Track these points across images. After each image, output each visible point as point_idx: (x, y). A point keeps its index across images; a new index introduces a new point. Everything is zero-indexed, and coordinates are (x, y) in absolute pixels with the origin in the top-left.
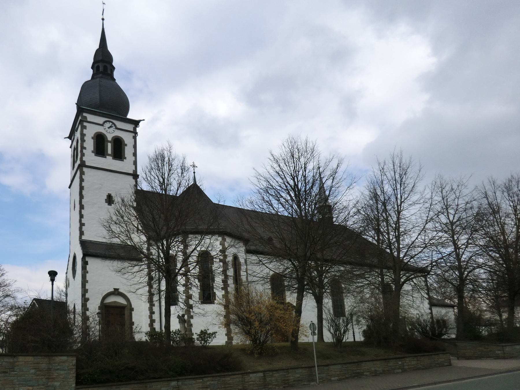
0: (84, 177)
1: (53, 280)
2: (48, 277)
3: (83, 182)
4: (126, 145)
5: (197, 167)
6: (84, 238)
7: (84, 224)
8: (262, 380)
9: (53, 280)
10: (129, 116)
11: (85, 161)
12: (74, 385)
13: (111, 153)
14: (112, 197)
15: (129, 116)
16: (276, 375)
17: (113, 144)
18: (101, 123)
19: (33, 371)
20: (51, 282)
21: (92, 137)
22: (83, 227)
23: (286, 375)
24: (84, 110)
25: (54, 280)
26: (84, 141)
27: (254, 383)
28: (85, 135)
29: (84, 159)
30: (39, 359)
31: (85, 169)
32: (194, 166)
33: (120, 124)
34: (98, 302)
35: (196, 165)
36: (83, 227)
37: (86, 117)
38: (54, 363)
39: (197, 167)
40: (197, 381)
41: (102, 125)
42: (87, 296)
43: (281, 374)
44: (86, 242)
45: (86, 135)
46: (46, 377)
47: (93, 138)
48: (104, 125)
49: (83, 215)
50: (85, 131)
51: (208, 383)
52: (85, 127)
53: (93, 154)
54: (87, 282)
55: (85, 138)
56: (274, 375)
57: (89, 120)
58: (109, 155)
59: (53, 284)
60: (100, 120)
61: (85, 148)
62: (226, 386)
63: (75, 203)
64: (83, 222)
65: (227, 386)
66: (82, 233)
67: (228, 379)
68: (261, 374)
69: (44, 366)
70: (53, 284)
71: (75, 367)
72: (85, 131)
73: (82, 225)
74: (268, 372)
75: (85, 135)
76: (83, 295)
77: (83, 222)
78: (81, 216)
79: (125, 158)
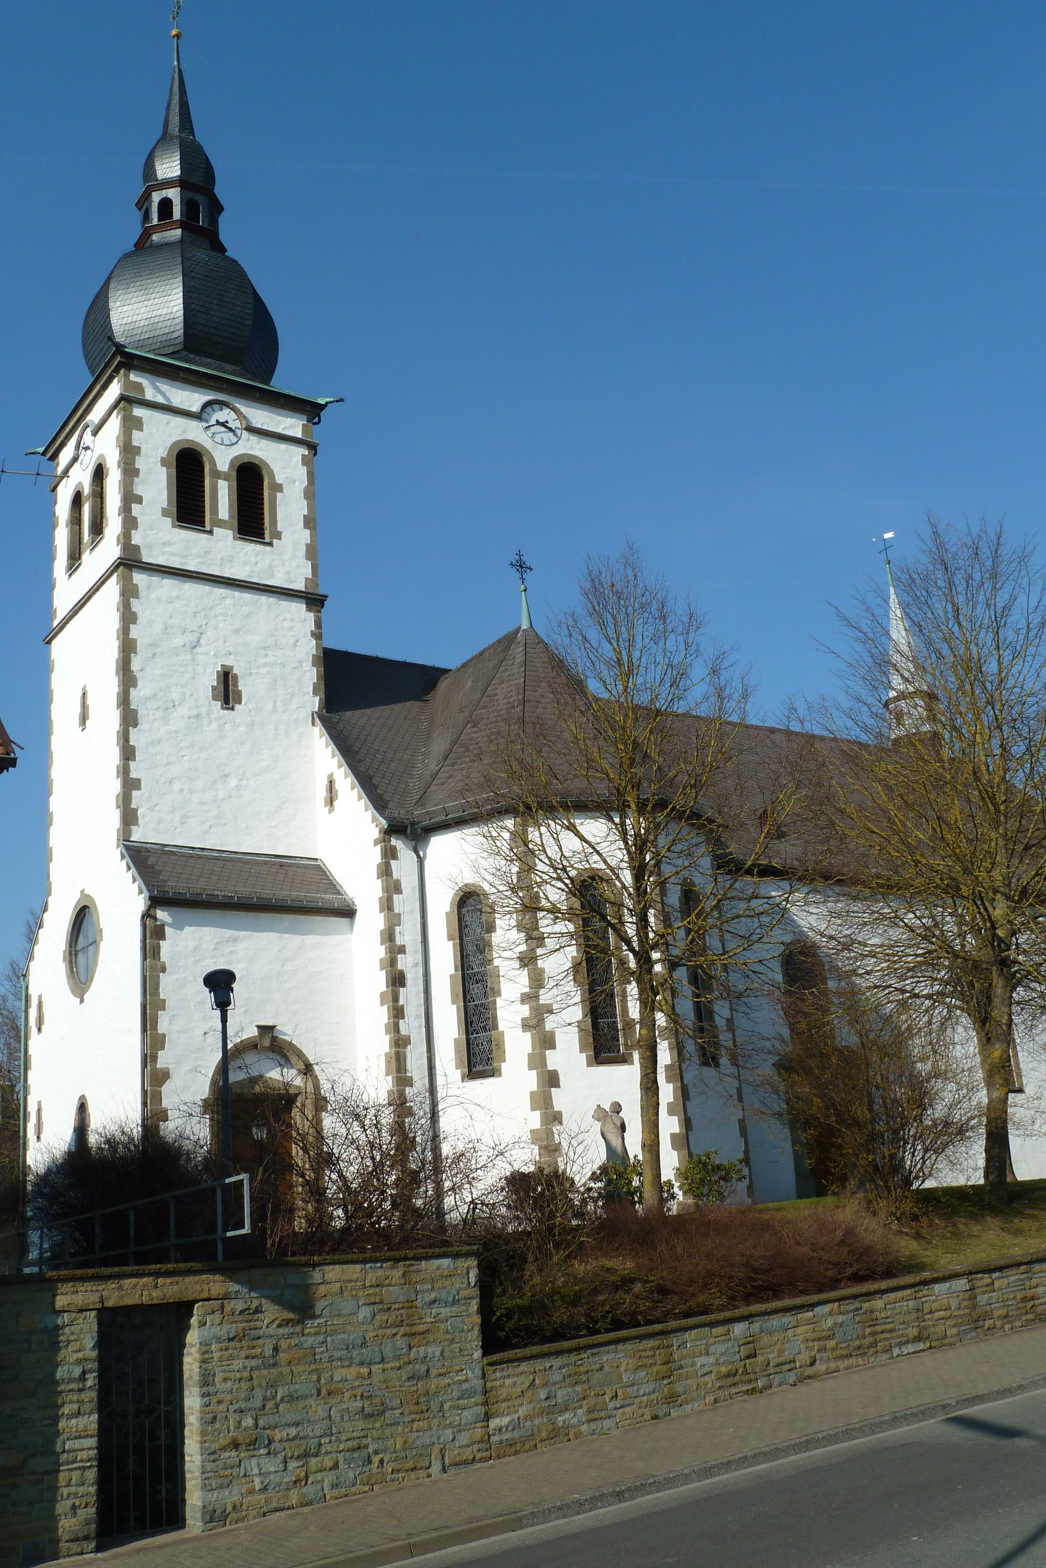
0: (135, 605)
1: (223, 1004)
2: (207, 997)
3: (135, 623)
4: (279, 488)
5: (512, 564)
6: (138, 835)
7: (139, 781)
8: (965, 1303)
9: (223, 1004)
10: (279, 383)
11: (137, 548)
12: (478, 1354)
13: (230, 516)
14: (236, 677)
15: (279, 383)
16: (1000, 1281)
17: (235, 484)
18: (195, 408)
19: (365, 1313)
20: (218, 1013)
21: (163, 460)
22: (135, 793)
23: (1027, 1283)
24: (136, 362)
25: (229, 1004)
26: (136, 473)
27: (947, 1313)
28: (137, 450)
29: (136, 539)
30: (374, 1273)
31: (139, 578)
32: (521, 567)
33: (262, 417)
34: (201, 1088)
35: (528, 562)
36: (135, 793)
37: (139, 387)
38: (422, 1281)
39: (531, 569)
40: (800, 1316)
41: (197, 416)
42: (163, 1060)
43: (1013, 1278)
44: (147, 850)
45: (143, 451)
46: (402, 1331)
47: (164, 462)
48: (204, 416)
49: (133, 748)
50: (137, 438)
51: (830, 1323)
52: (137, 424)
53: (168, 521)
54: (162, 1005)
55: (140, 463)
56: (997, 1285)
57: (150, 395)
58: (221, 524)
59: (224, 1020)
60: (193, 399)
61: (139, 500)
62: (878, 1329)
63: (89, 702)
64: (133, 775)
65: (882, 1327)
66: (129, 817)
67: (878, 1303)
68: (962, 1284)
69: (394, 1293)
70: (224, 1020)
71: (476, 1292)
72: (137, 438)
73: (130, 785)
74: (980, 1276)
75: (137, 450)
76: (148, 1059)
77: (133, 775)
78: (128, 753)
79: (278, 535)
